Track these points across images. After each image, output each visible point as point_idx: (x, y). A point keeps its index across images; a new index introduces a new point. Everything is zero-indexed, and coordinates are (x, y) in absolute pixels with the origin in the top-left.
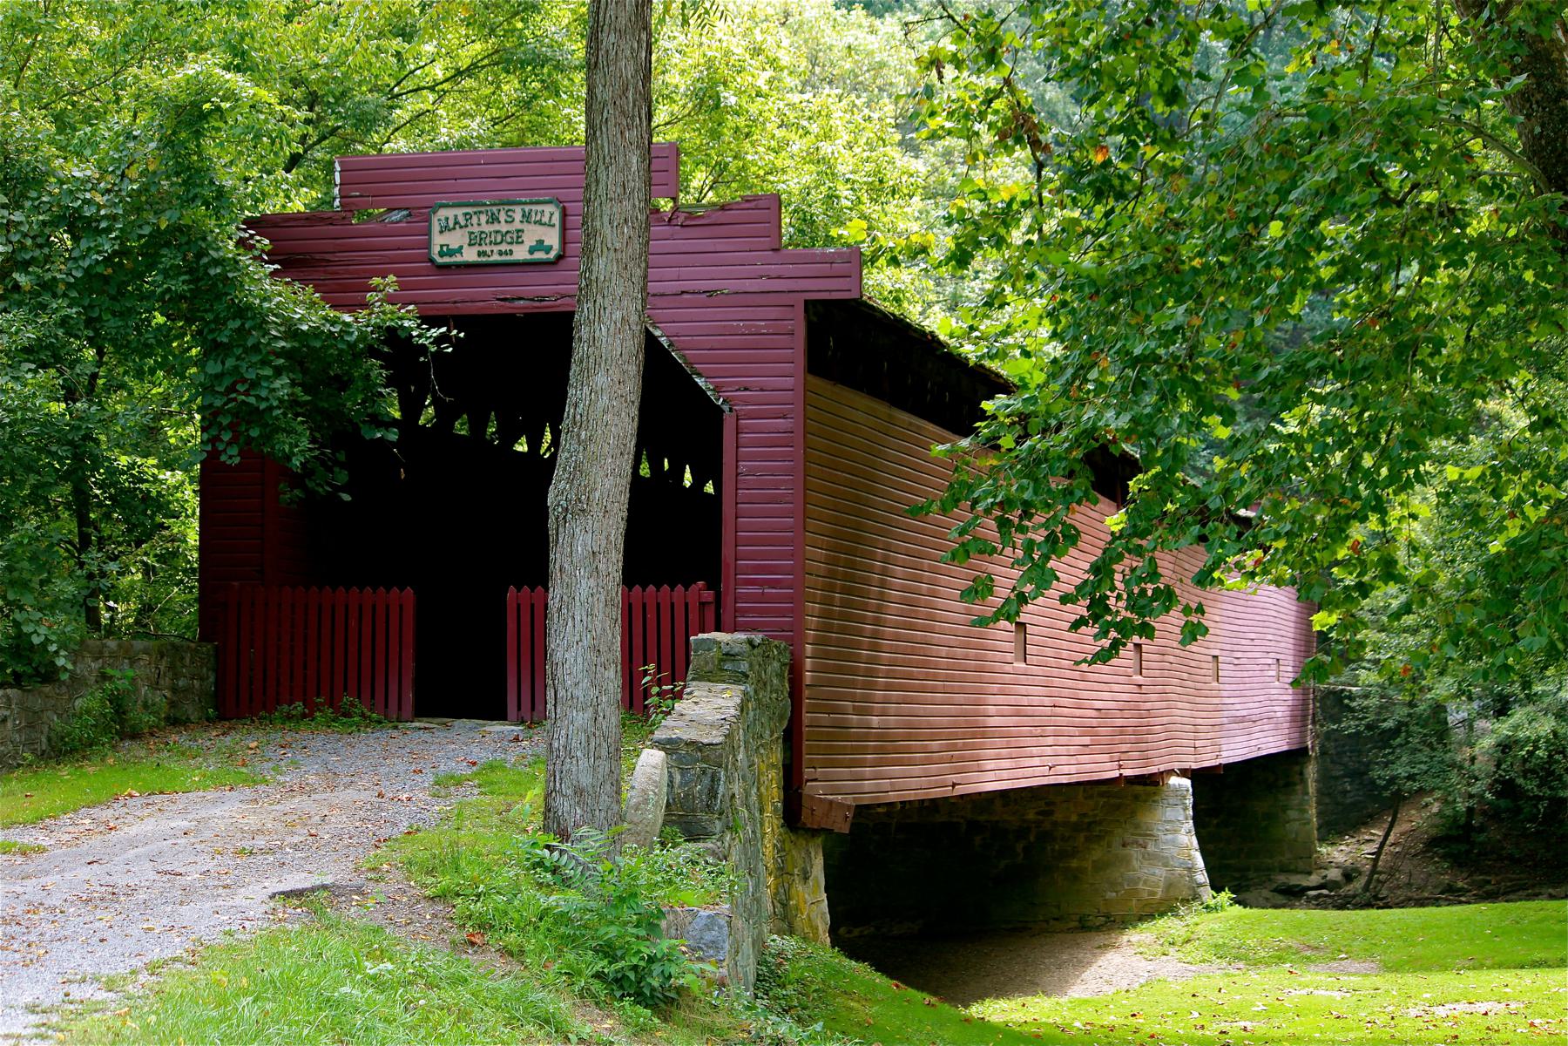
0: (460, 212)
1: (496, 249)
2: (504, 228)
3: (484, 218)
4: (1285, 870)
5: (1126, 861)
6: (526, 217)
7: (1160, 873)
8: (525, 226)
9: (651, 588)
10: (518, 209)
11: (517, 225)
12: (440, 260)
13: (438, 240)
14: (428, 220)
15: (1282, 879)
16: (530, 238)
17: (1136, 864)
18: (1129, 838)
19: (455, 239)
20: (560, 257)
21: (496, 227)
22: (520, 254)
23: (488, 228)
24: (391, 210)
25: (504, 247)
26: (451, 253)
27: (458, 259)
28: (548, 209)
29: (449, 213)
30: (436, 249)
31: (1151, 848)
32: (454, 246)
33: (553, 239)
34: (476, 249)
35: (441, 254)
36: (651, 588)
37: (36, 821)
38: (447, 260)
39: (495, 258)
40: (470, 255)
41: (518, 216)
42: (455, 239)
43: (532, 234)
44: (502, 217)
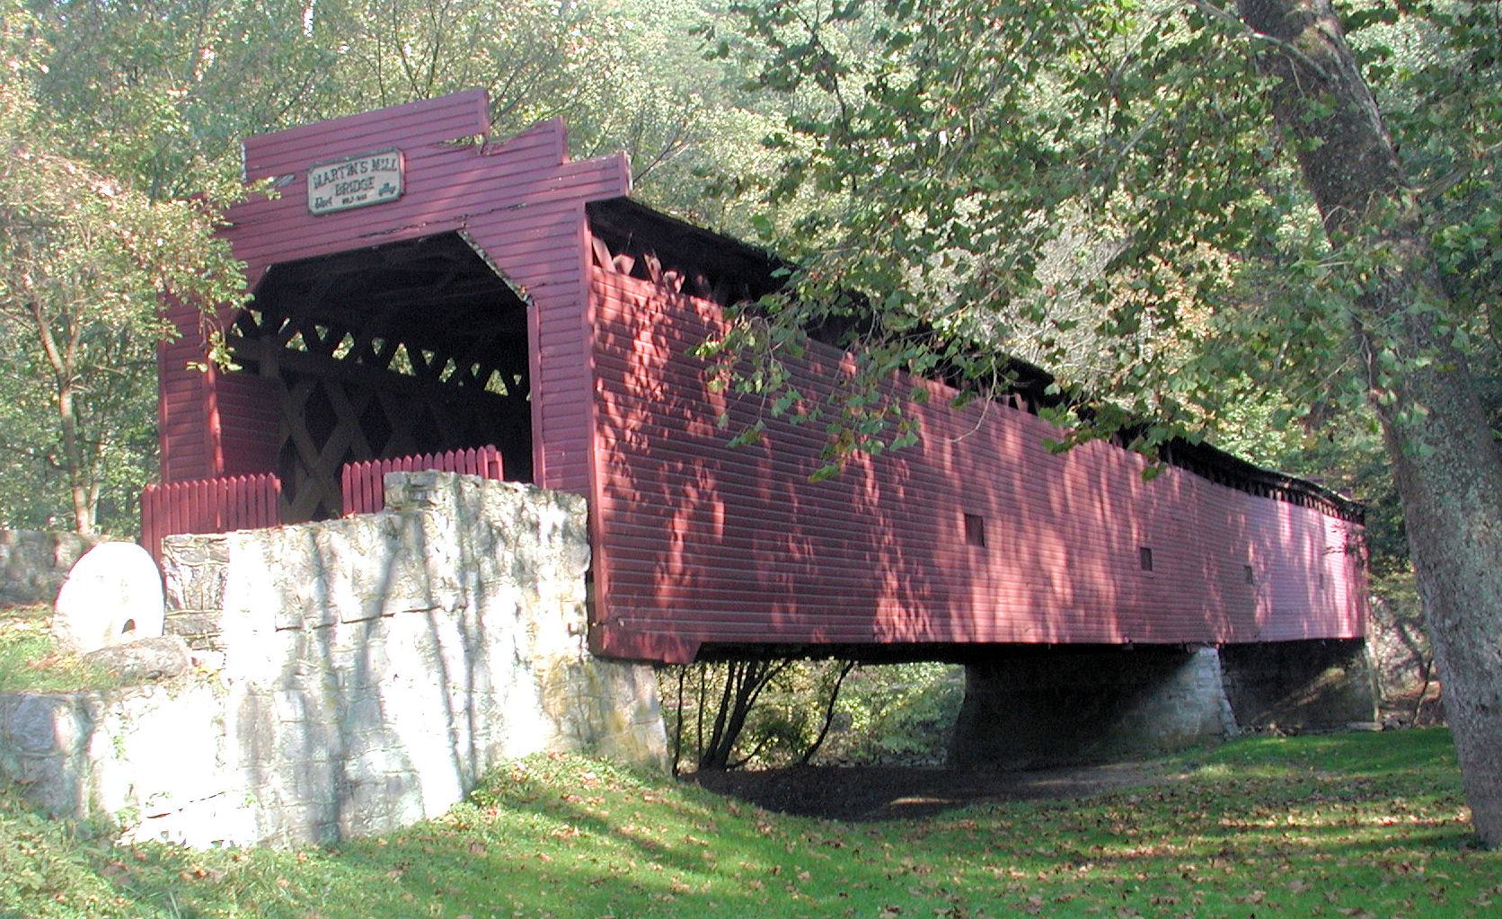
0: (328, 169)
1: (355, 195)
2: (360, 177)
3: (346, 172)
4: (1356, 720)
5: (1172, 709)
6: (375, 166)
7: (1197, 716)
8: (376, 174)
9: (450, 453)
10: (370, 161)
11: (370, 173)
12: (315, 210)
13: (314, 195)
14: (306, 181)
15: (1354, 725)
16: (378, 185)
17: (1179, 711)
18: (1172, 692)
19: (326, 192)
20: (402, 195)
21: (355, 177)
22: (372, 196)
23: (348, 179)
24: (281, 176)
25: (360, 193)
26: (323, 204)
27: (328, 208)
28: (391, 156)
29: (320, 171)
30: (312, 203)
31: (1189, 698)
32: (326, 198)
33: (395, 182)
34: (342, 197)
35: (317, 206)
36: (450, 453)
37: (1418, 759)
38: (321, 209)
39: (356, 203)
40: (337, 203)
41: (370, 167)
42: (326, 192)
43: (381, 179)
44: (359, 168)
